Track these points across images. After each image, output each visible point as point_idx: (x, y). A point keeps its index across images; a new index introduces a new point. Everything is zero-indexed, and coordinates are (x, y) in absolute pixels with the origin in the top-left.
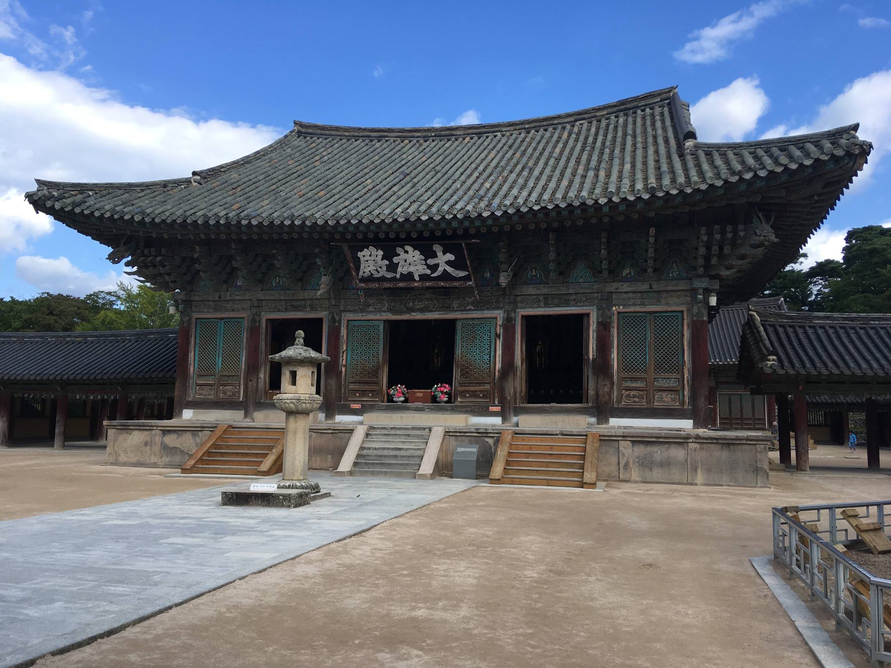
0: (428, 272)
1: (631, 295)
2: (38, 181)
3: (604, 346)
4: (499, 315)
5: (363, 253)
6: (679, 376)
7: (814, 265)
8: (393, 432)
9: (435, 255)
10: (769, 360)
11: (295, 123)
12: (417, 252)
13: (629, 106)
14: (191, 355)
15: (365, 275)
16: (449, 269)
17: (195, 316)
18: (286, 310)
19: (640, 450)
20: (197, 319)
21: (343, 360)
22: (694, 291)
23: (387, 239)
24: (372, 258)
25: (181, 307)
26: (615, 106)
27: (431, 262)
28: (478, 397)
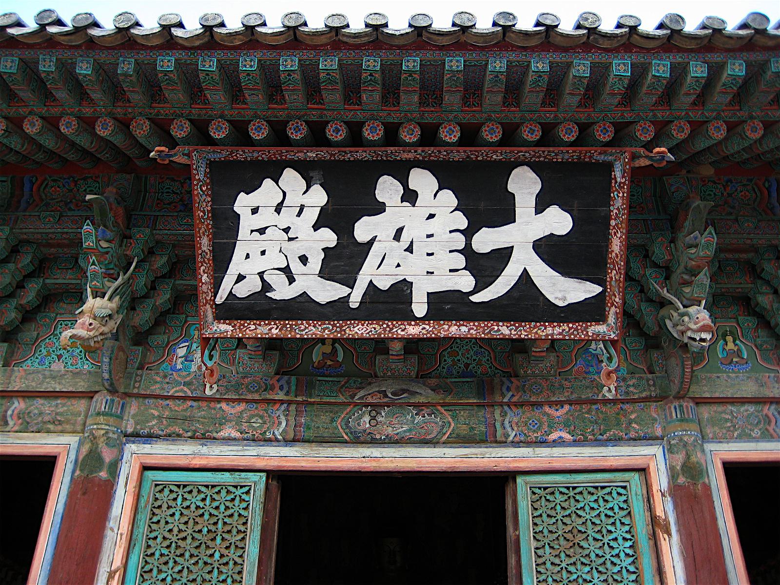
0: (465, 282)
9: (505, 214)
12: (449, 198)
15: (243, 291)
27: (487, 240)
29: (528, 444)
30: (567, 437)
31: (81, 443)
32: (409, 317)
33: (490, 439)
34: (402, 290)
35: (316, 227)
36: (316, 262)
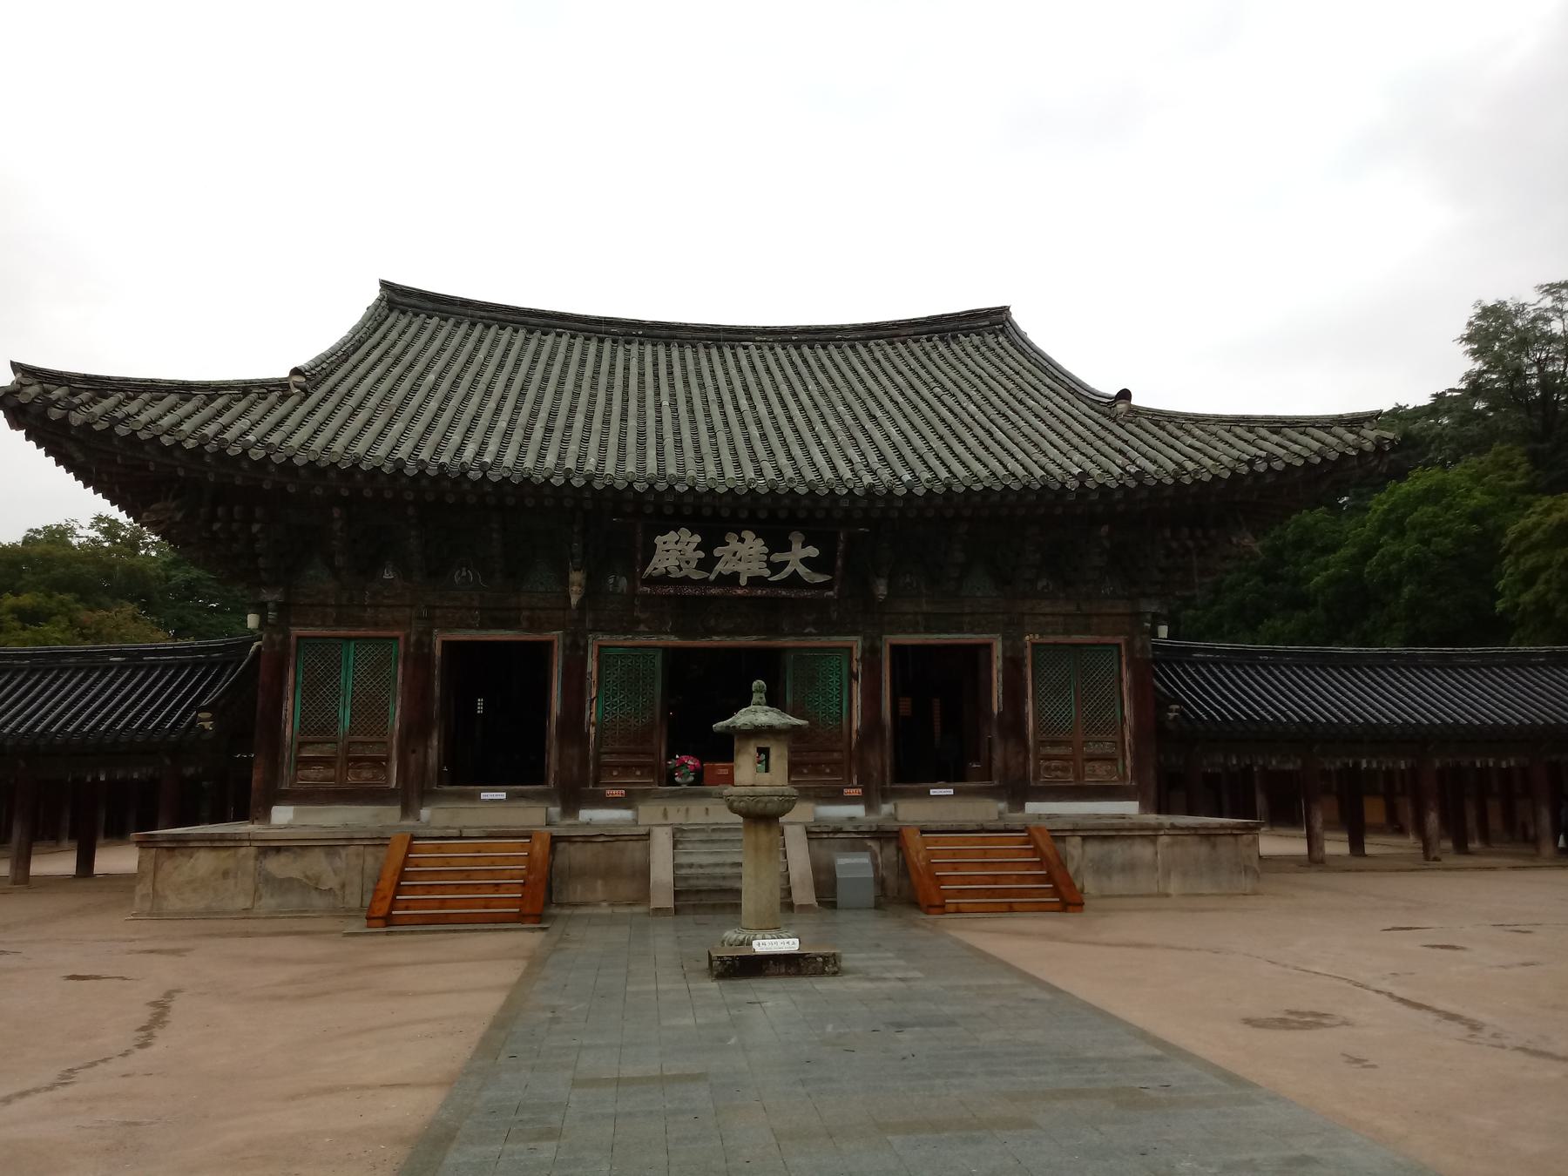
0: (767, 573)
1: (1050, 619)
2: (16, 367)
3: (1014, 694)
4: (856, 643)
5: (665, 538)
6: (1116, 738)
7: (32, 444)
8: (715, 836)
12: (761, 542)
13: (946, 327)
14: (288, 705)
16: (803, 570)
17: (296, 631)
18: (482, 626)
19: (1094, 849)
20: (299, 638)
21: (592, 714)
22: (1138, 616)
24: (679, 547)
25: (271, 615)
27: (777, 557)
28: (823, 773)
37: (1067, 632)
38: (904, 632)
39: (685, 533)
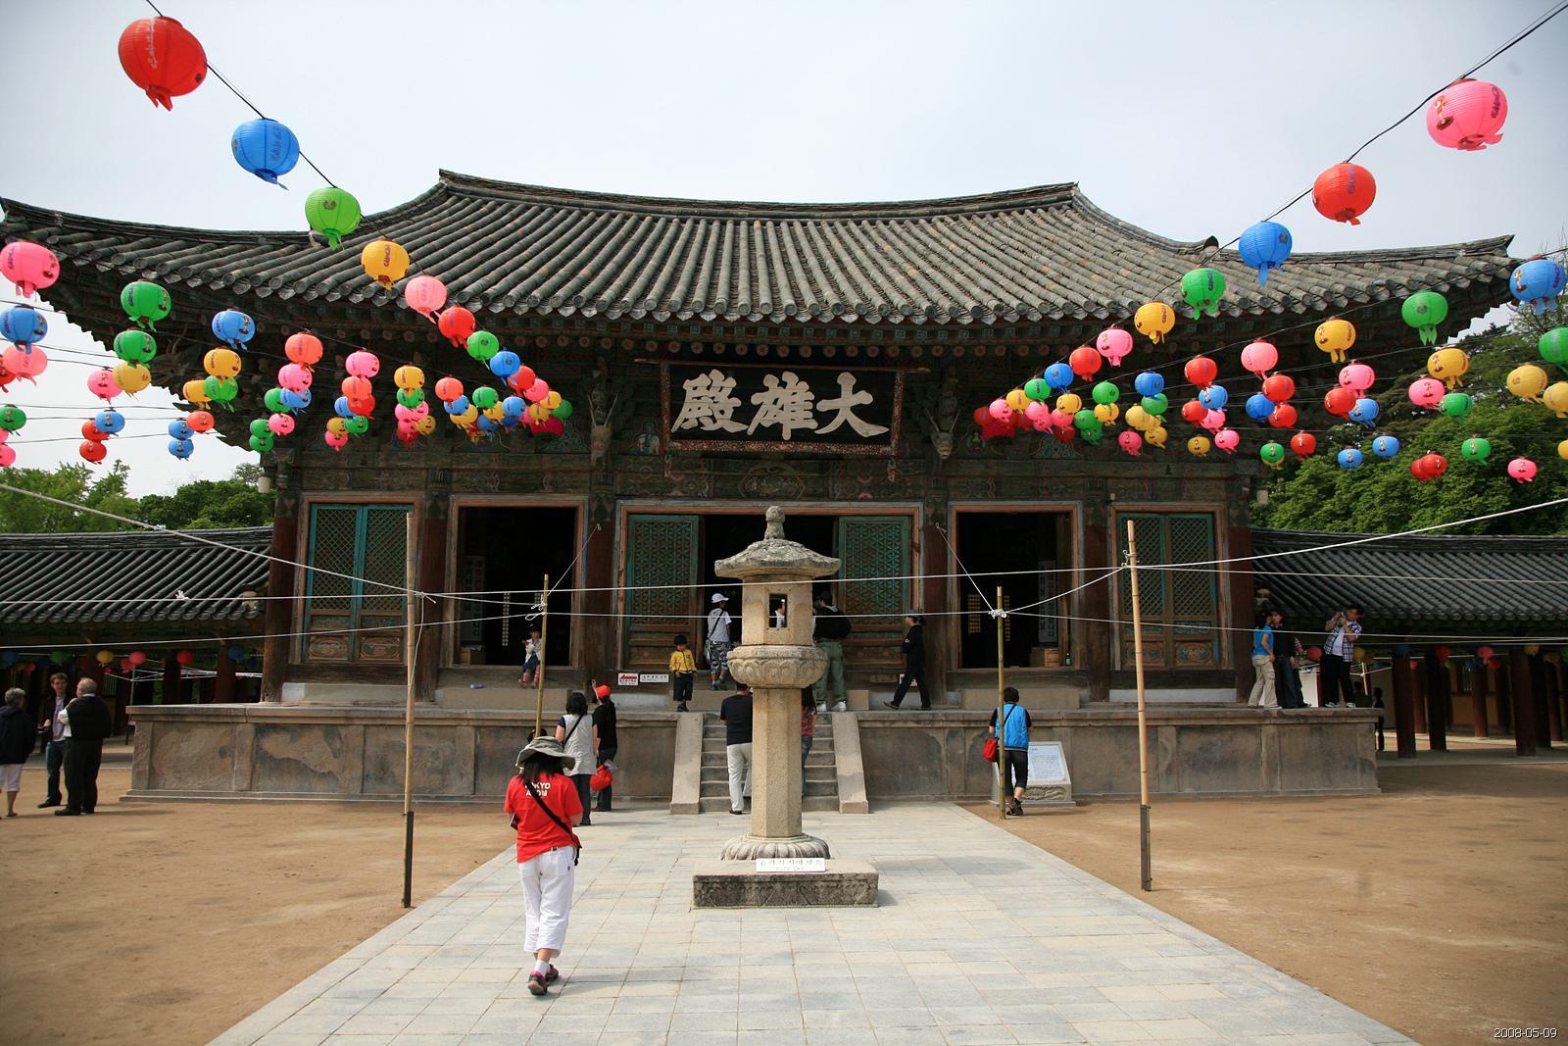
0: (813, 424)
10: (1260, 596)
11: (442, 173)
12: (804, 385)
15: (687, 426)
18: (502, 490)
23: (752, 355)
26: (990, 200)
27: (824, 405)
29: (847, 500)
30: (870, 496)
31: (591, 501)
32: (780, 439)
33: (826, 496)
34: (777, 428)
35: (729, 397)
36: (729, 413)
37: (1155, 498)
38: (973, 498)
39: (716, 375)
